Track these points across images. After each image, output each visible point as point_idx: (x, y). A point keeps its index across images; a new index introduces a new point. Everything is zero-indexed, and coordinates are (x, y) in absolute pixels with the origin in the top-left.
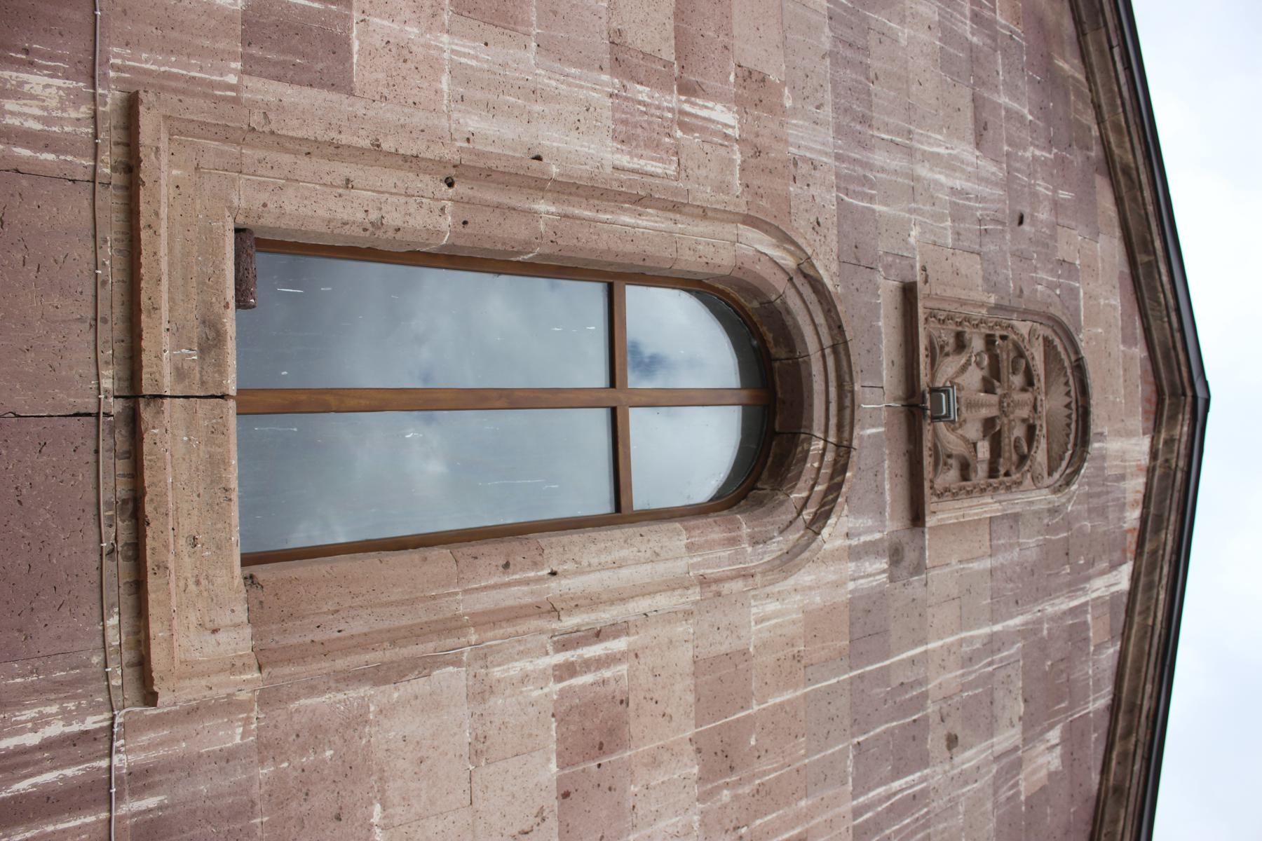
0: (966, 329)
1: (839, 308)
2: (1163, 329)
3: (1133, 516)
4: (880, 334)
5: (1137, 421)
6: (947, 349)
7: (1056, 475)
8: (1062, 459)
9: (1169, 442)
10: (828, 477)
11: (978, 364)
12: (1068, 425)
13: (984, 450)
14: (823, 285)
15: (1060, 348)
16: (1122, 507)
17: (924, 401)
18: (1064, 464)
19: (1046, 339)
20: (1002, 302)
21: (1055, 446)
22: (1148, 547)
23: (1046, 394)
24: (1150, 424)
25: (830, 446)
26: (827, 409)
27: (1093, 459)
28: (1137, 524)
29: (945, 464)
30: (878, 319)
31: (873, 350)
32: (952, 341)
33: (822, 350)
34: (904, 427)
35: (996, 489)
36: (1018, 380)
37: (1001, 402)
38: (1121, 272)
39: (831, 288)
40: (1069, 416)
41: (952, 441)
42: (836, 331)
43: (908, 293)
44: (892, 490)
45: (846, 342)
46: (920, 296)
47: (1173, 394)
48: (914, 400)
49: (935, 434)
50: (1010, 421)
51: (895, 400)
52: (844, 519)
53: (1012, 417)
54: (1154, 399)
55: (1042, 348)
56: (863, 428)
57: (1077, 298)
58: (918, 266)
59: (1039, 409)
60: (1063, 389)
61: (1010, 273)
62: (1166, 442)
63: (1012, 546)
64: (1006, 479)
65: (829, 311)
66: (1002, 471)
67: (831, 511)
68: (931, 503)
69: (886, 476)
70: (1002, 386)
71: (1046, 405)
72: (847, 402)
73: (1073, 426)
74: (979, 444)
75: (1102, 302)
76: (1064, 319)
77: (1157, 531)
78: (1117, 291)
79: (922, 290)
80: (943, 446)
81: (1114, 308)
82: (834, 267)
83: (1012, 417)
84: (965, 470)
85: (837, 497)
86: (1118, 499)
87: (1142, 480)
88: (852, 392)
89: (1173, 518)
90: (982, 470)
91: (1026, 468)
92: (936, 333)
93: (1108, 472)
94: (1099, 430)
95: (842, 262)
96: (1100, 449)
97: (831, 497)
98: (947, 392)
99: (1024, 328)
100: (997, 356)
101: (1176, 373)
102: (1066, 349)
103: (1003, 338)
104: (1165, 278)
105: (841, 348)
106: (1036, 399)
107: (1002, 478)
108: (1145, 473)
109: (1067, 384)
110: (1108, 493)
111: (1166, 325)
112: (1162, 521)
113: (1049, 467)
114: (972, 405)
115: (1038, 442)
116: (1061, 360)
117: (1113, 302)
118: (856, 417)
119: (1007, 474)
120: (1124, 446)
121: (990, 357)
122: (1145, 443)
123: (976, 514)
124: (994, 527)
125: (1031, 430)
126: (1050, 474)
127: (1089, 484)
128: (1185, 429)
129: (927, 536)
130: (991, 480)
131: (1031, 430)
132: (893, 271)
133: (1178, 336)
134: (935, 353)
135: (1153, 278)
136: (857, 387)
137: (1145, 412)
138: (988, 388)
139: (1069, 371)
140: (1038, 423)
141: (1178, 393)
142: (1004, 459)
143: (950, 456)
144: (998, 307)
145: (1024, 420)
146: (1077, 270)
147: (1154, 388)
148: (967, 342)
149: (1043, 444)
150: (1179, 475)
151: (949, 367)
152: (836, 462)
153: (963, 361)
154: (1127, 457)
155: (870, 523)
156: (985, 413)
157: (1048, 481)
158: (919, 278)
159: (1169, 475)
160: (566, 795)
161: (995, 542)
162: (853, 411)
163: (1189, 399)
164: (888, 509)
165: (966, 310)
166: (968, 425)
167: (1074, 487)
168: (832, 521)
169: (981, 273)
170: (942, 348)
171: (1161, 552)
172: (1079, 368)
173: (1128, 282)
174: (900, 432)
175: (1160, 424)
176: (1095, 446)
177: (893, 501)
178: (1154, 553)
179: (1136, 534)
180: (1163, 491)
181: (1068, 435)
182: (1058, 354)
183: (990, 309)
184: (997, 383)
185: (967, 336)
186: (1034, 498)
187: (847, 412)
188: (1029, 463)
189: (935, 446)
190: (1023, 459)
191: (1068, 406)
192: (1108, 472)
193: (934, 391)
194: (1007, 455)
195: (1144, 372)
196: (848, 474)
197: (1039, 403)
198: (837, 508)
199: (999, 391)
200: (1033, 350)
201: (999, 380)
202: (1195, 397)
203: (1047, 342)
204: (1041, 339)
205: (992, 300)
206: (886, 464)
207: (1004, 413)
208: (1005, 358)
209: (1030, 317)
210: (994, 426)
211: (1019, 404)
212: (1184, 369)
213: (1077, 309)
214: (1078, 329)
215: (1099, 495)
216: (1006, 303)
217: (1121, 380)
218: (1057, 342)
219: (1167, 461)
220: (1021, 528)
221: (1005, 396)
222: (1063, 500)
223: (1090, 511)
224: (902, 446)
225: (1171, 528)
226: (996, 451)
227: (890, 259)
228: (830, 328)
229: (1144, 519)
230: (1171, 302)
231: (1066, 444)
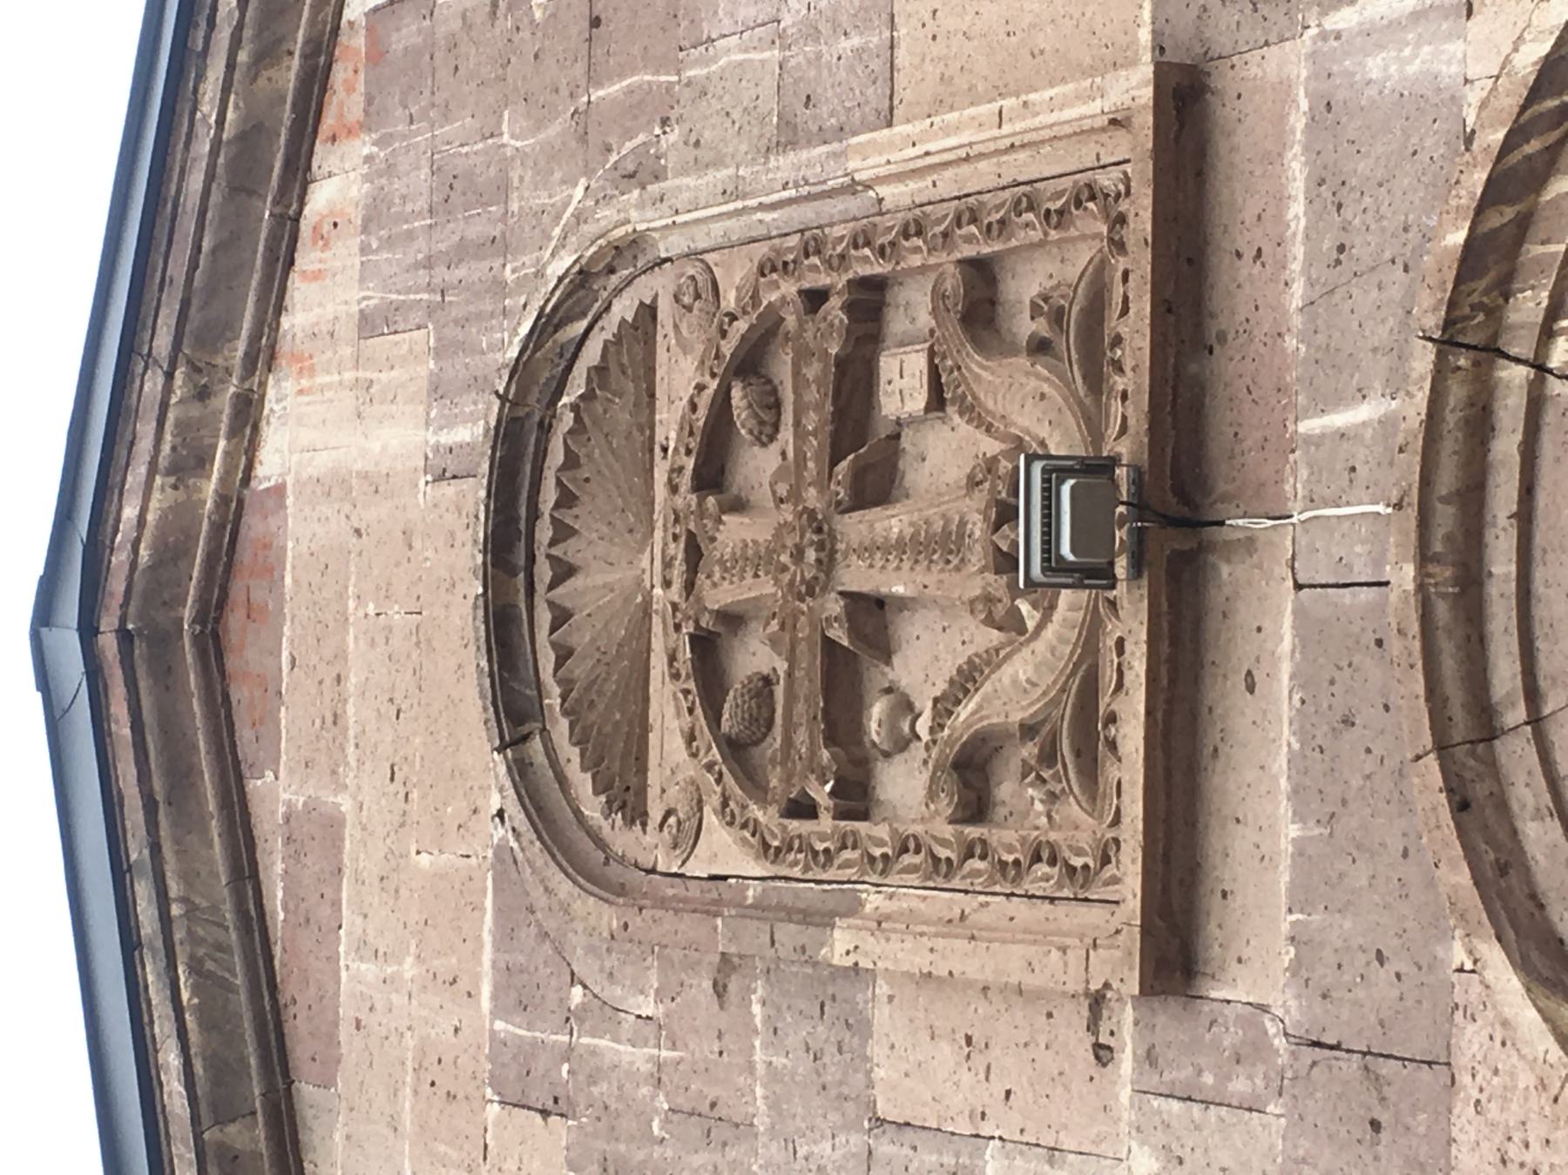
0: (948, 831)
1: (1464, 877)
2: (187, 877)
3: (337, 186)
4: (1296, 792)
5: (301, 535)
6: (1029, 751)
7: (624, 309)
8: (600, 372)
9: (188, 463)
10: (1539, 229)
11: (906, 706)
12: (566, 499)
13: (901, 382)
14: (1522, 965)
15: (582, 783)
16: (375, 215)
17: (1139, 536)
18: (592, 353)
19: (636, 814)
20: (807, 935)
21: (621, 414)
22: (289, 74)
23: (646, 610)
24: (253, 525)
25: (1522, 346)
26: (1528, 490)
27: (476, 383)
28: (324, 157)
29: (1058, 318)
30: (1300, 848)
31: (1330, 723)
32: (1006, 789)
33: (1536, 720)
34: (1218, 443)
35: (862, 239)
36: (754, 656)
37: (828, 563)
38: (327, 1083)
39: (1495, 958)
40: (563, 532)
41: (1031, 405)
42: (1480, 790)
43: (1174, 956)
44: (1280, 198)
45: (1442, 747)
46: (1132, 938)
47: (163, 641)
48: (1180, 541)
49: (1093, 426)
50: (795, 495)
51: (1250, 543)
52: (1482, 68)
53: (787, 514)
54: (235, 619)
55: (654, 778)
56: (1387, 423)
57: (507, 973)
58: (1126, 1063)
59: (678, 550)
60: (580, 635)
61: (759, 1056)
62: (202, 462)
63: (812, 33)
64: (823, 280)
65: (1503, 869)
66: (834, 307)
67: (1536, 92)
68: (1131, 159)
69: (1299, 250)
70: (820, 625)
71: (651, 565)
72: (1446, 518)
73: (549, 495)
74: (918, 402)
75: (409, 969)
76: (564, 887)
77: (253, 135)
78: (346, 1011)
79: (1121, 969)
80: (1068, 384)
81: (361, 947)
82: (1471, 1041)
83: (787, 514)
84: (978, 305)
85: (1507, 146)
86: (389, 243)
87: (294, 321)
88: (1424, 557)
89: (196, 182)
90: (914, 310)
91: (742, 326)
92: (1072, 809)
93: (423, 339)
94: (449, 490)
95: (1440, 1062)
96: (449, 423)
97: (1533, 146)
98: (1053, 562)
99: (722, 850)
100: (831, 739)
101: (148, 716)
102: (562, 779)
103: (803, 809)
104: (170, 1058)
105: (1461, 727)
106: (689, 586)
107: (840, 280)
108: (284, 347)
109: (564, 655)
110: (429, 264)
111: (174, 889)
112: (232, 165)
113: (649, 342)
114: (938, 545)
115: (687, 428)
116: (580, 738)
117: (369, 969)
118: (1412, 463)
119: (815, 299)
120: (362, 442)
121: (858, 727)
122: (271, 464)
123: (947, 131)
124: (875, 96)
125: (712, 471)
126: (648, 312)
127: (499, 288)
128: (130, 512)
129: (1145, 36)
130: (879, 268)
131: (712, 471)
132: (1231, 1038)
133: (137, 851)
134: (1073, 735)
135: (211, 1061)
136: (1405, 576)
137: (271, 571)
138: (873, 616)
139: (553, 700)
140: (687, 498)
141: (161, 638)
142: (821, 351)
143: (1040, 347)
144: (820, 919)
145: (738, 506)
146: (494, 1082)
147: (231, 662)
148: (949, 781)
149: (668, 423)
150: (163, 342)
151: (1024, 682)
152: (1505, 289)
153: (964, 712)
154: (348, 400)
155: (1374, 67)
156: (893, 522)
157: (658, 286)
158: (1124, 1020)
159: (200, 340)
160: (475, 811)
161: (876, 40)
162: (1426, 481)
163: (108, 622)
164: (1298, 122)
165: (944, 903)
166: (956, 473)
167: (561, 265)
168: (1537, 49)
169: (876, 1050)
170: (1049, 756)
171: (243, 57)
172: (514, 715)
173: (301, 1050)
174: (1236, 421)
175: (217, 528)
176: (472, 429)
177: (1275, 158)
178: (268, 55)
179: (328, 122)
180: (224, 281)
181: (571, 461)
182: (592, 763)
183: (853, 908)
184: (839, 634)
185: (945, 806)
186: (713, 208)
187: (1447, 479)
188: (728, 348)
189: (1095, 382)
190: (749, 363)
191: (564, 571)
192: (423, 339)
193: (1095, 575)
194: (812, 371)
195: (267, 722)
196: (1457, 237)
197: (678, 572)
198: (1510, 102)
199: (834, 606)
200: (690, 769)
201: (829, 645)
202: (88, 630)
203: (628, 801)
204: (655, 813)
205: (840, 945)
206: (1297, 295)
207: (816, 524)
208: (797, 734)
209: (694, 890)
210: (858, 475)
211: (757, 560)
212: (122, 729)
213: (506, 935)
214: (504, 860)
215: (463, 252)
216: (789, 934)
217: (352, 682)
218: (592, 807)
219: (202, 394)
220: (769, 104)
221: (811, 589)
222: (607, 214)
223: (503, 189)
224: (1231, 368)
225: (203, 147)
226: (854, 382)
227: (1239, 1086)
228: (1502, 805)
229: (298, 173)
230: (152, 975)
231: (579, 428)
